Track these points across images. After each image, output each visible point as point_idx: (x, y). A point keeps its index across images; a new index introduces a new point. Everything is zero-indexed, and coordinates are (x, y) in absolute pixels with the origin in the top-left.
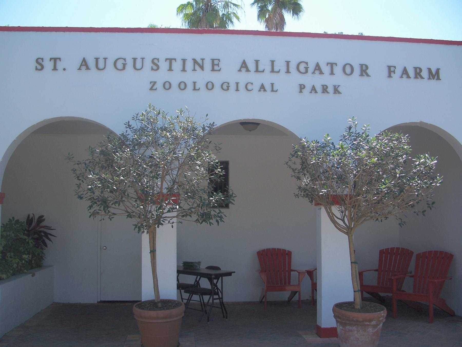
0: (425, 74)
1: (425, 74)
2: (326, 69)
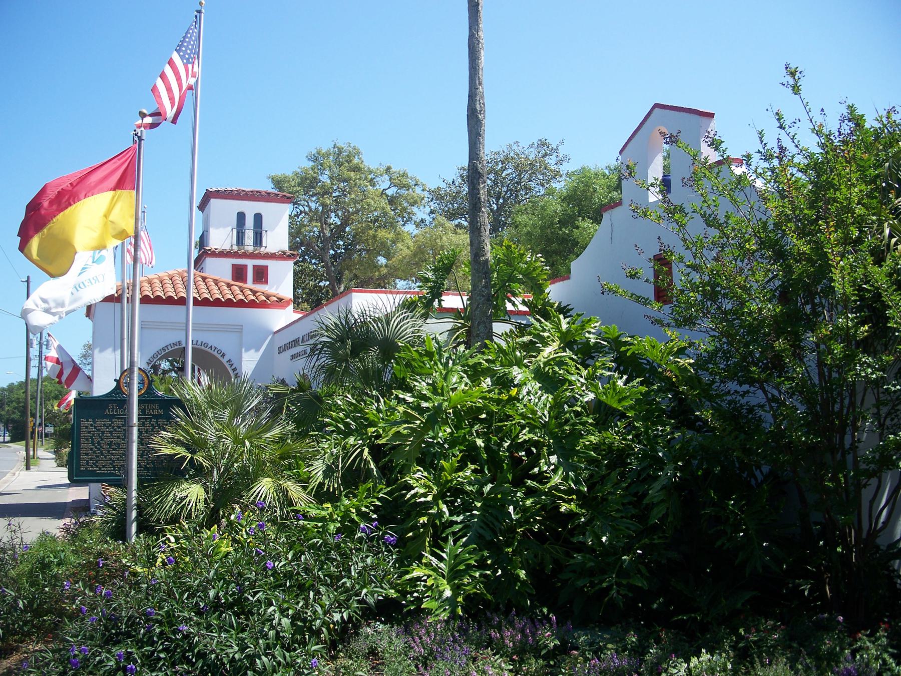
0: (235, 372)
1: (235, 372)
2: (213, 349)
